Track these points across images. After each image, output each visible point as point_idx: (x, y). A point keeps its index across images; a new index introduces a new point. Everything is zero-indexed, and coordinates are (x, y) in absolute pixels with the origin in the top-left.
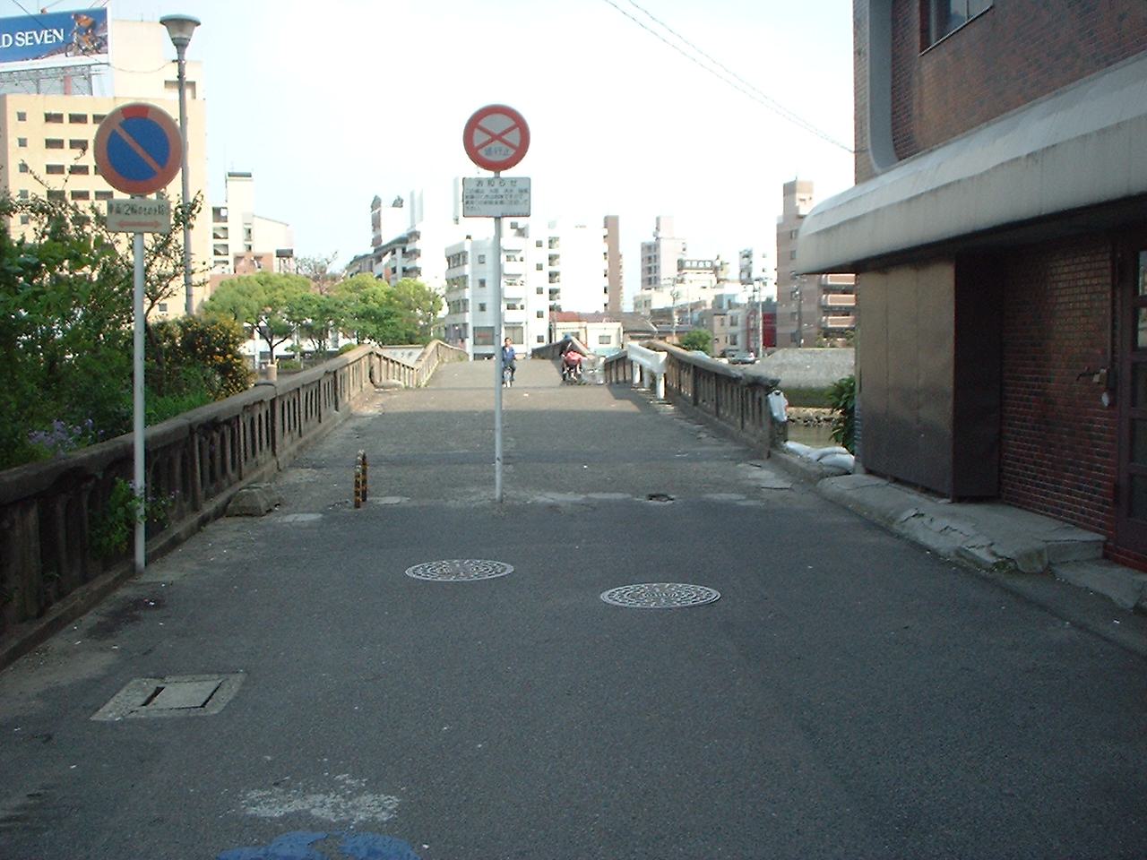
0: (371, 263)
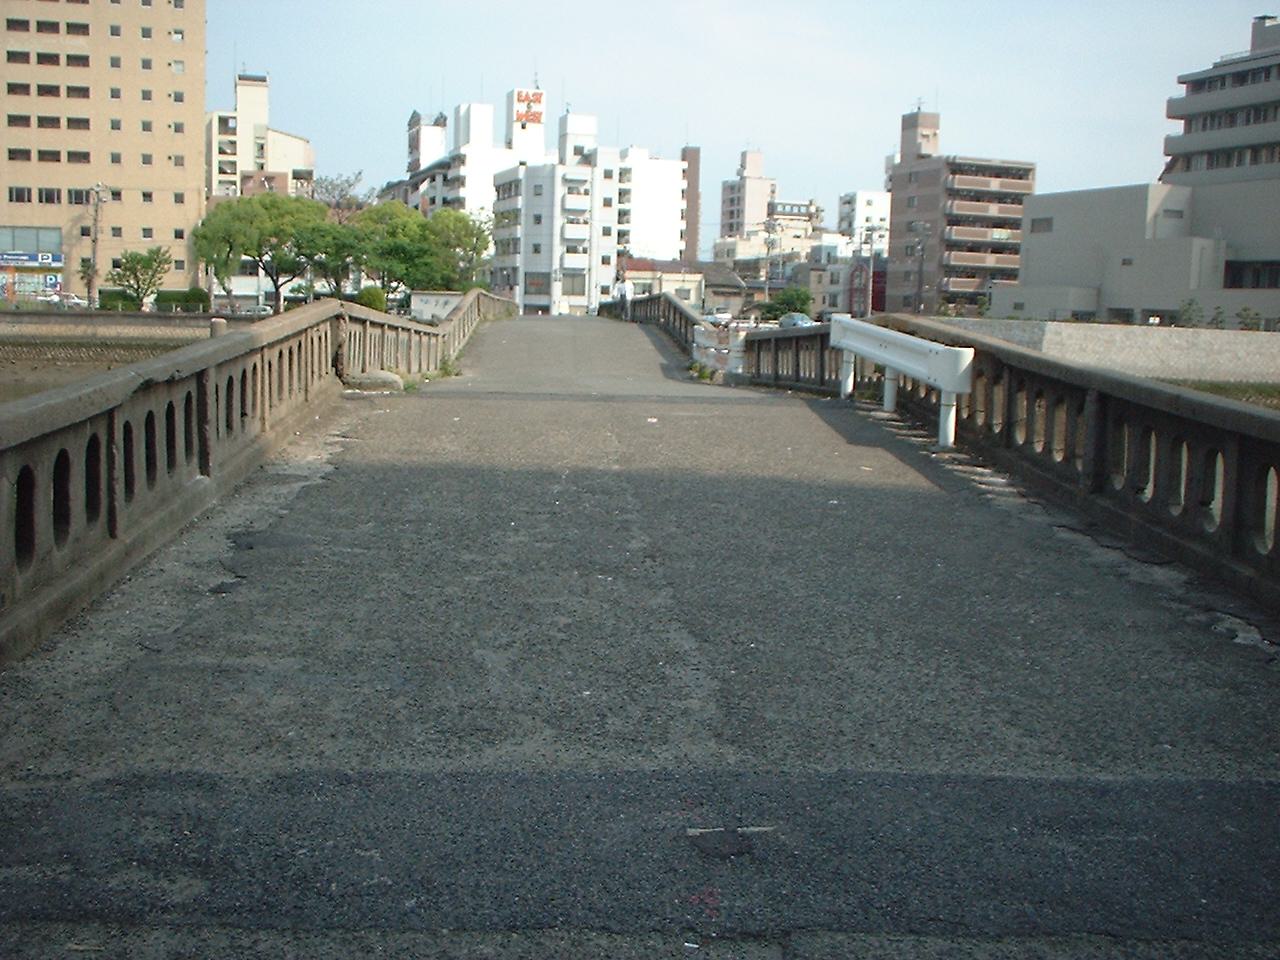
0: (406, 191)
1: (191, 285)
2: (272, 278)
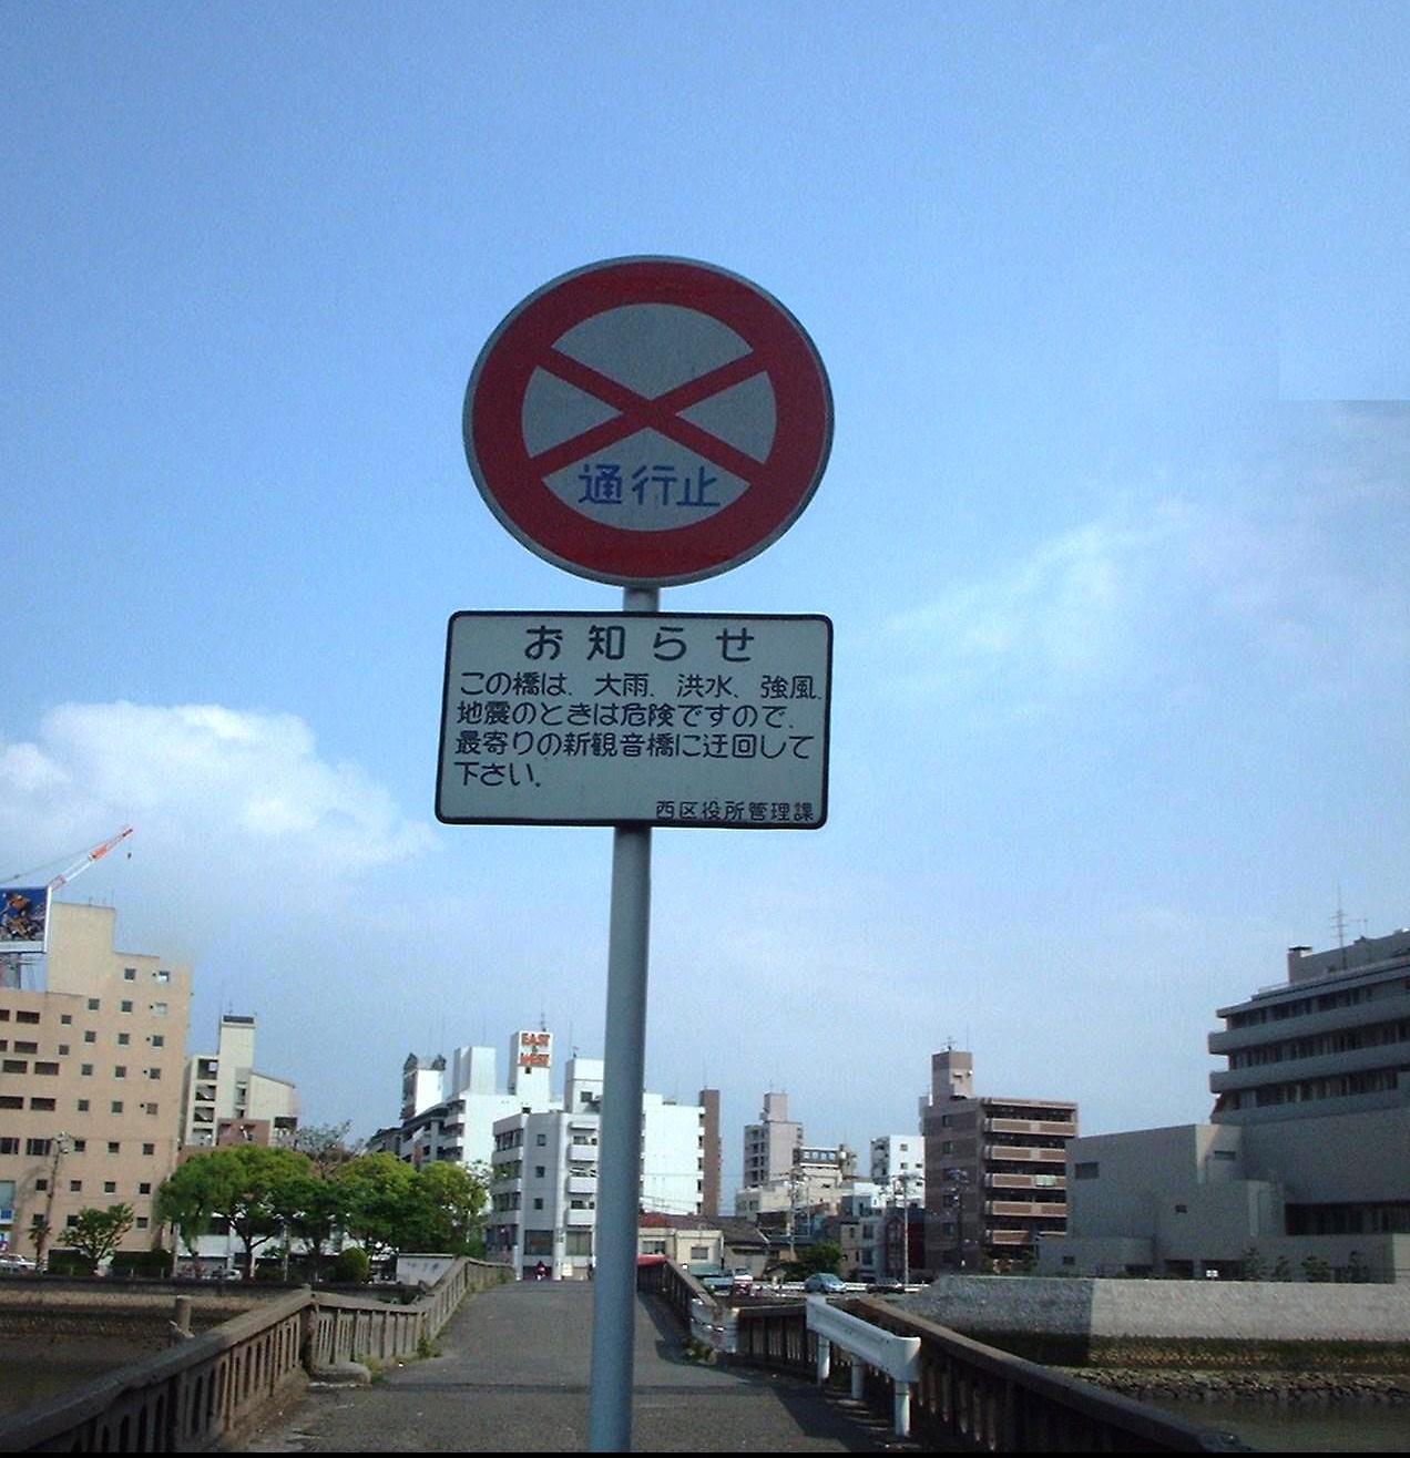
0: (398, 1139)
1: (154, 1244)
2: (244, 1238)
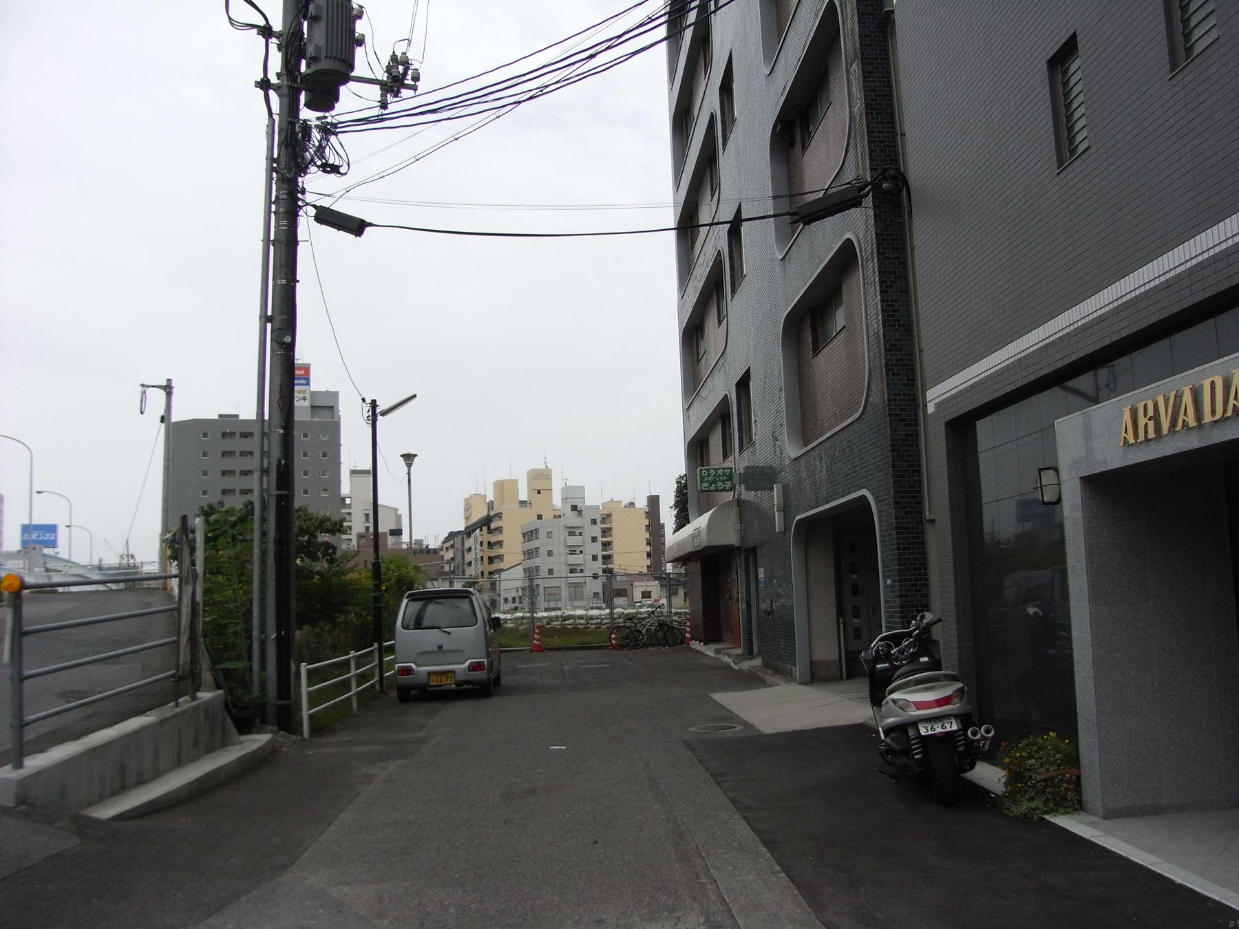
0: (463, 537)
